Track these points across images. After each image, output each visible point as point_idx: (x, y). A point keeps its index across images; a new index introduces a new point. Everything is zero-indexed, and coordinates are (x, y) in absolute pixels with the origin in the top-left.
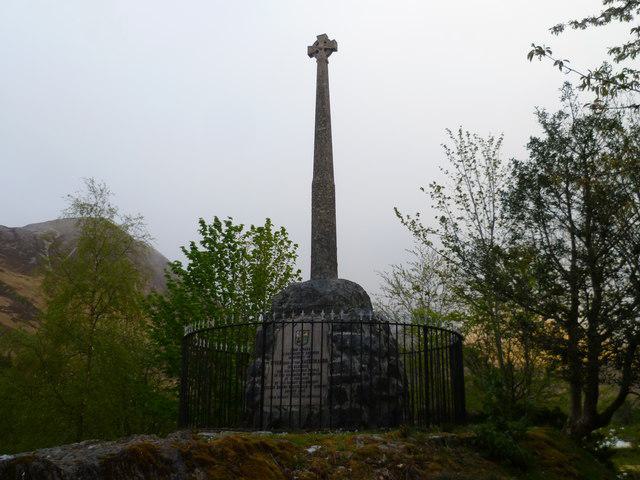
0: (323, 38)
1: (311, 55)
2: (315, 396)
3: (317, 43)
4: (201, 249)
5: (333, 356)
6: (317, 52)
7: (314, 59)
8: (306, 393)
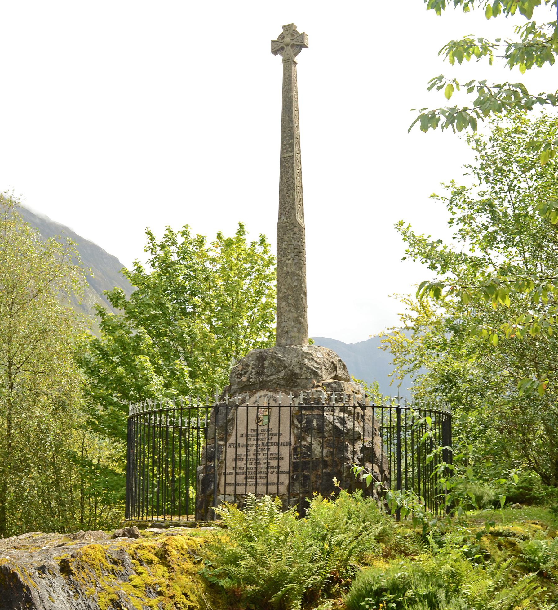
0: (289, 29)
1: (275, 52)
2: (283, 473)
3: (282, 37)
4: (148, 271)
5: (300, 438)
6: (282, 48)
7: (301, 32)
8: (273, 478)
